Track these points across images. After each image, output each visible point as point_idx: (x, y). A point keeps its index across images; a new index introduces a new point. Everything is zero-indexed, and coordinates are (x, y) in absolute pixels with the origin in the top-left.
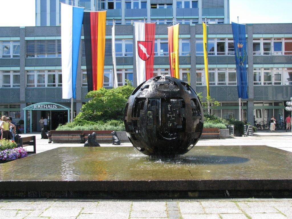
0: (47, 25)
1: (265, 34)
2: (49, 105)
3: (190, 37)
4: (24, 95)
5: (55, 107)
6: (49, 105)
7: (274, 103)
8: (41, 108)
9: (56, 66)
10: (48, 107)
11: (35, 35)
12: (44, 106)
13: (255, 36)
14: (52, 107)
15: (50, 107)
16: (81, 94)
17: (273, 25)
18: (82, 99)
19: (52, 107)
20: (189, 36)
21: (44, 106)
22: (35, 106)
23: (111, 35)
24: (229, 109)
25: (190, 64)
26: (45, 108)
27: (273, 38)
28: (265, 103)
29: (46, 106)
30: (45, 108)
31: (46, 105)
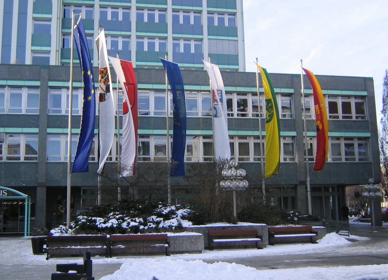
5: (5, 194)
18: (46, 180)
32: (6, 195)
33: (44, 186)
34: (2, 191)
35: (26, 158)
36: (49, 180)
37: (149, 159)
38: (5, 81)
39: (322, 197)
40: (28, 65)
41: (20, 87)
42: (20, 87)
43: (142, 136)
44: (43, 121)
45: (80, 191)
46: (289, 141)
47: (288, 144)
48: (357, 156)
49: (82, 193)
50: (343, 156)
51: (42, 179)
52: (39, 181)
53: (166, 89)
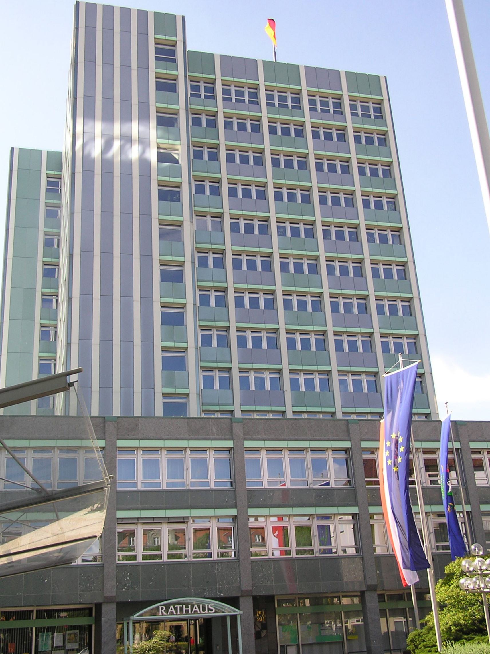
0: (192, 416)
1: (269, 440)
2: (172, 607)
3: (104, 446)
4: (114, 583)
5: (212, 610)
6: (172, 607)
7: (37, 611)
8: (176, 612)
9: (269, 507)
10: (194, 609)
11: (140, 436)
12: (184, 606)
13: (473, 445)
14: (204, 609)
15: (197, 609)
16: (252, 577)
17: (483, 423)
18: (253, 587)
19: (204, 609)
20: (229, 444)
21: (184, 606)
22: (162, 609)
23: (379, 441)
24: (350, 611)
25: (235, 506)
26: (187, 611)
27: (422, 450)
28: (343, 597)
29: (189, 609)
30: (187, 611)
31: (190, 606)
32: (213, 611)
33: (387, 590)
34: (208, 606)
35: (144, 557)
36: (256, 587)
37: (330, 551)
38: (54, 441)
39: (406, 609)
40: (33, 416)
41: (203, 450)
42: (203, 450)
43: (122, 521)
44: (242, 499)
45: (274, 601)
46: (227, 524)
47: (225, 529)
48: (140, 552)
49: (276, 606)
50: (293, 546)
51: (247, 585)
52: (243, 588)
53: (414, 441)
